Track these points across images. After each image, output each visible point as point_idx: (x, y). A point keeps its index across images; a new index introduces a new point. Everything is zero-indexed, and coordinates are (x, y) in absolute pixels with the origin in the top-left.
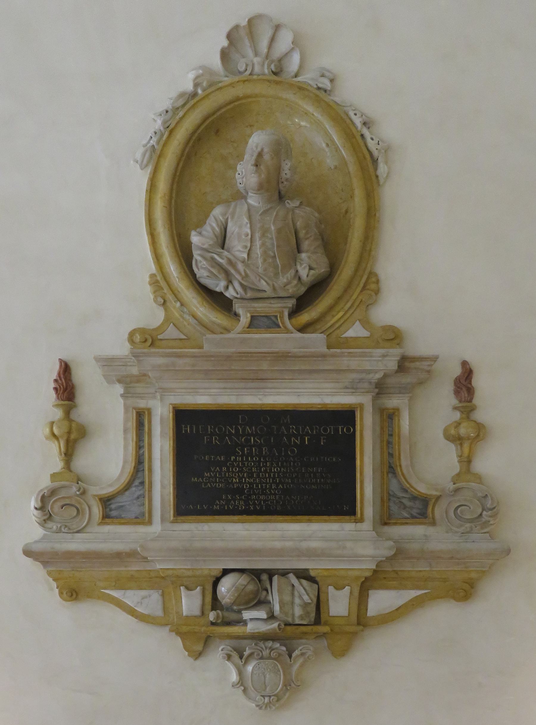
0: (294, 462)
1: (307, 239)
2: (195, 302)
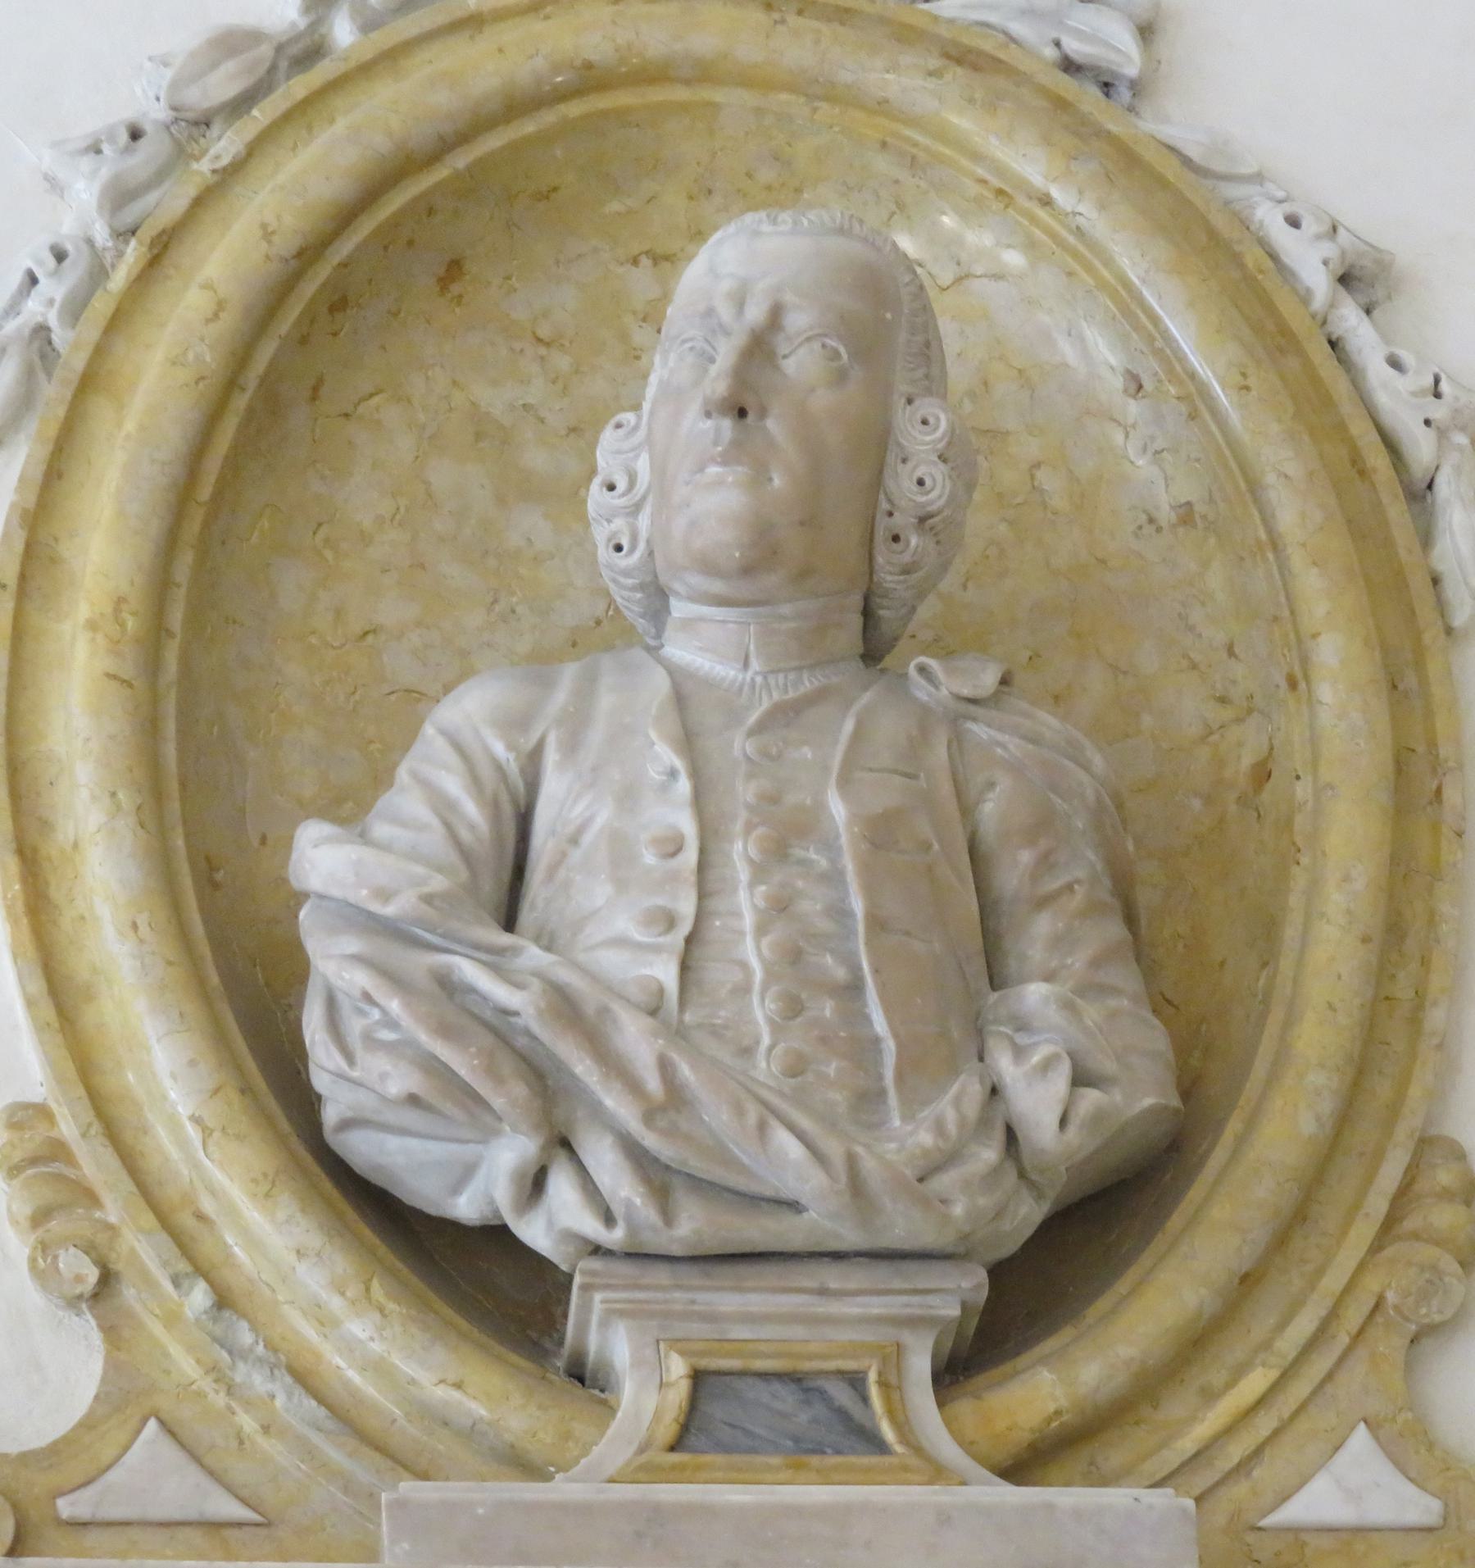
1: (1043, 902)
2: (313, 1279)
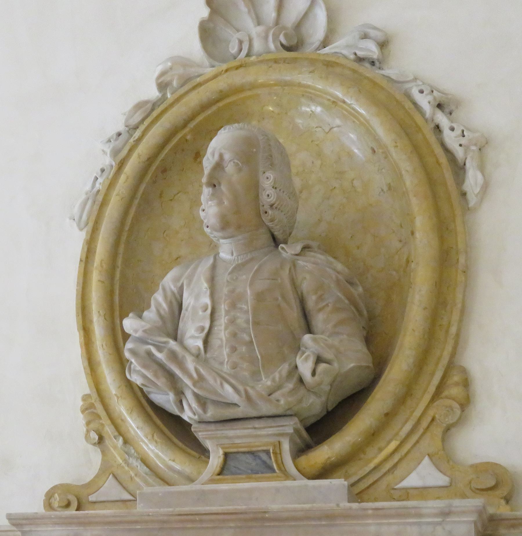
1: (320, 310)
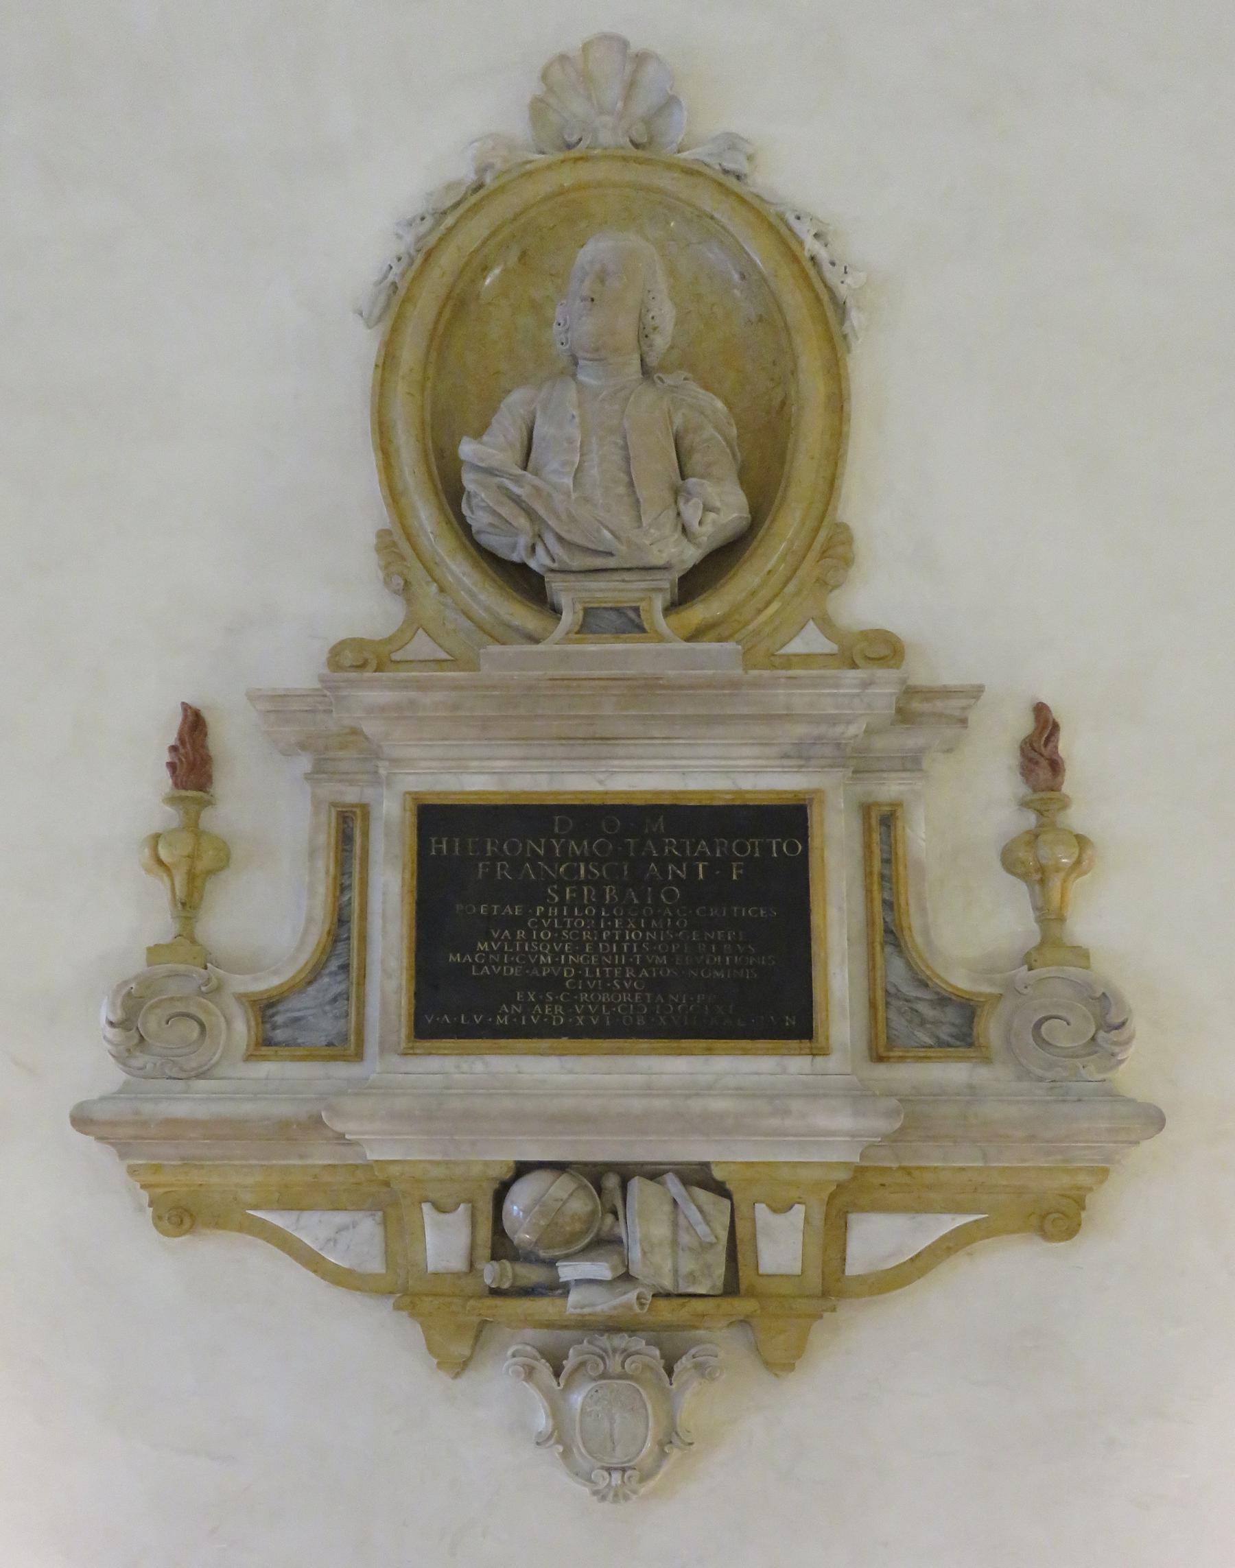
0: (674, 918)
